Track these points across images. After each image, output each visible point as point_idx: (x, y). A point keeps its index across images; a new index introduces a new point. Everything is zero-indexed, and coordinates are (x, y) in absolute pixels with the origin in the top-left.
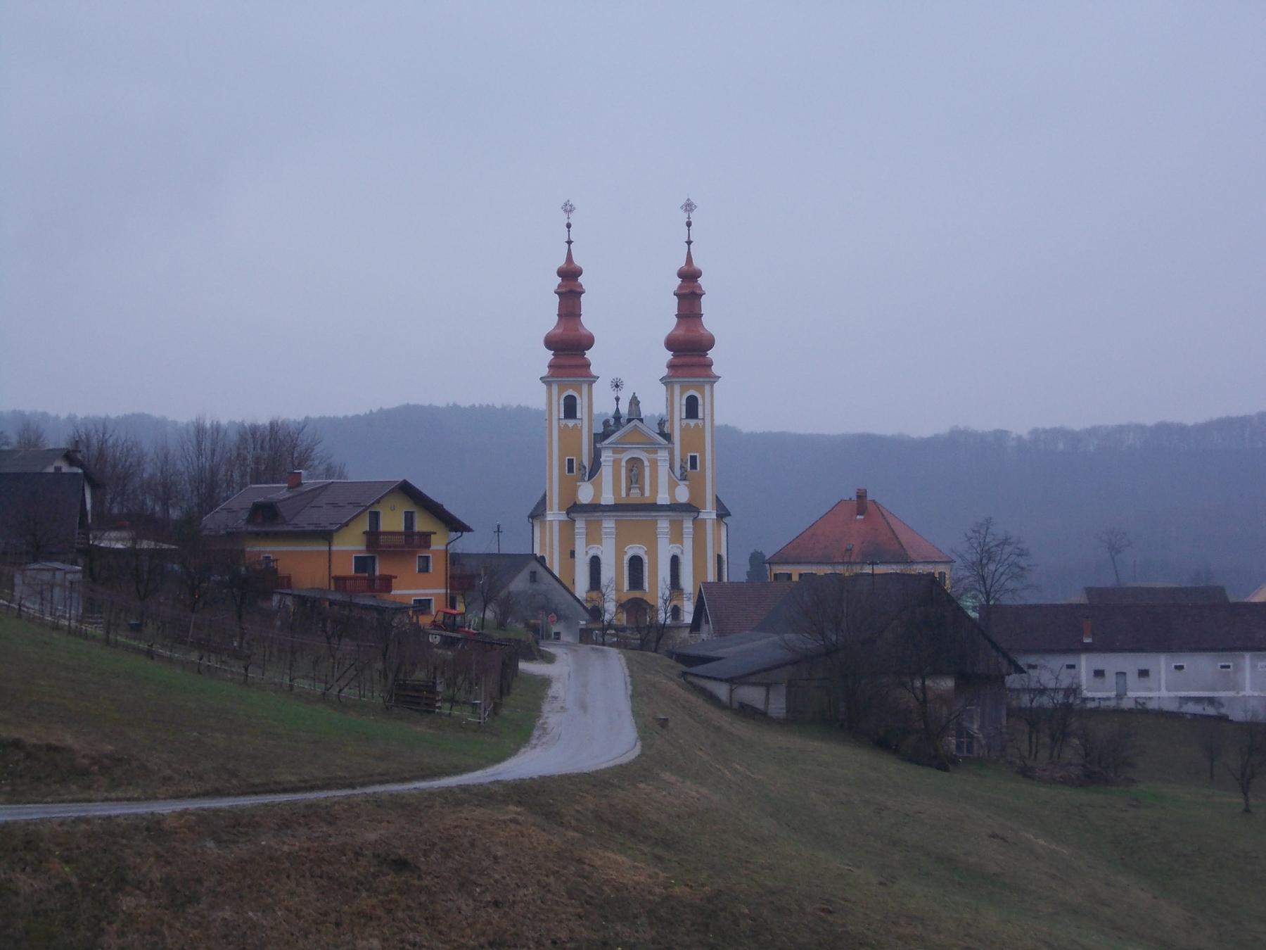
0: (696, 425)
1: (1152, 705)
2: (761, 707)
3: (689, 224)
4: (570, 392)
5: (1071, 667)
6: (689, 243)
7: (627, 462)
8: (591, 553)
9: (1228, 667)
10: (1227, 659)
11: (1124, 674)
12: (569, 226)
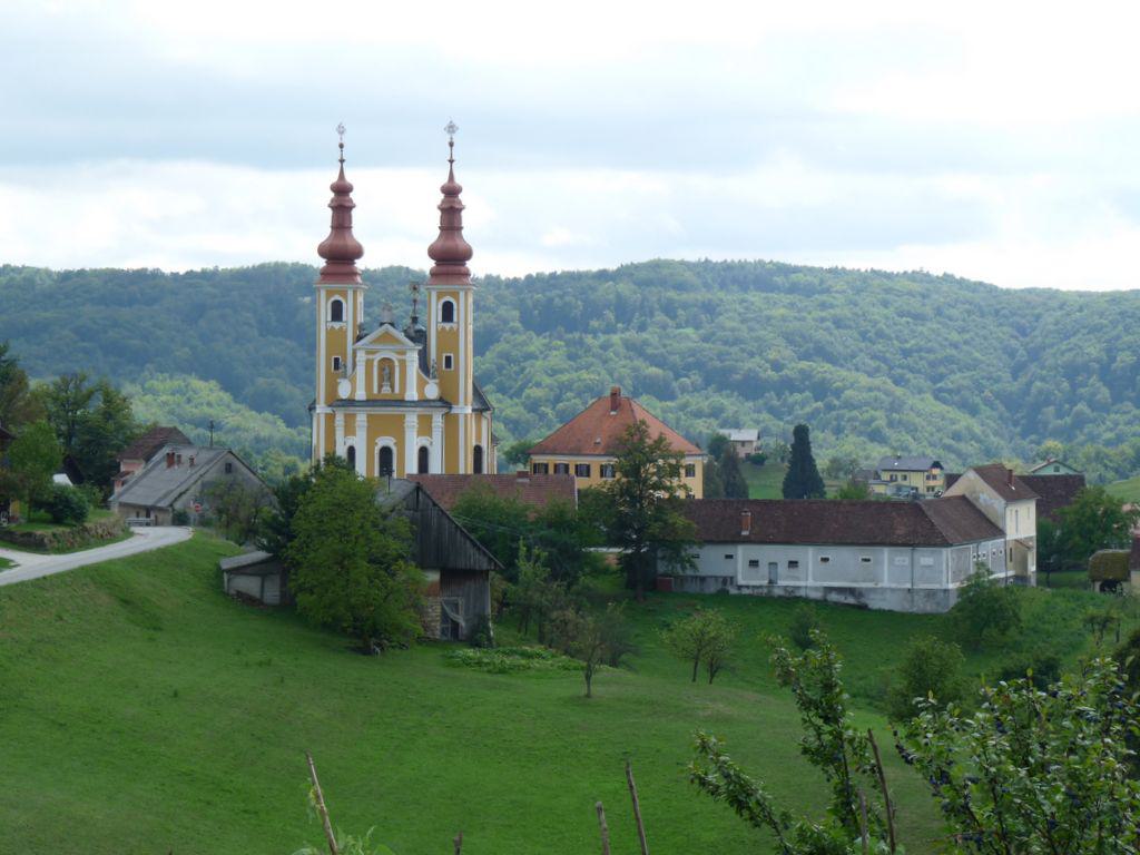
0: (452, 328)
1: (802, 593)
2: (258, 595)
3: (451, 145)
4: (337, 297)
5: (729, 557)
6: (451, 161)
7: (380, 361)
8: (348, 445)
9: (869, 560)
10: (867, 552)
11: (776, 564)
12: (341, 146)
